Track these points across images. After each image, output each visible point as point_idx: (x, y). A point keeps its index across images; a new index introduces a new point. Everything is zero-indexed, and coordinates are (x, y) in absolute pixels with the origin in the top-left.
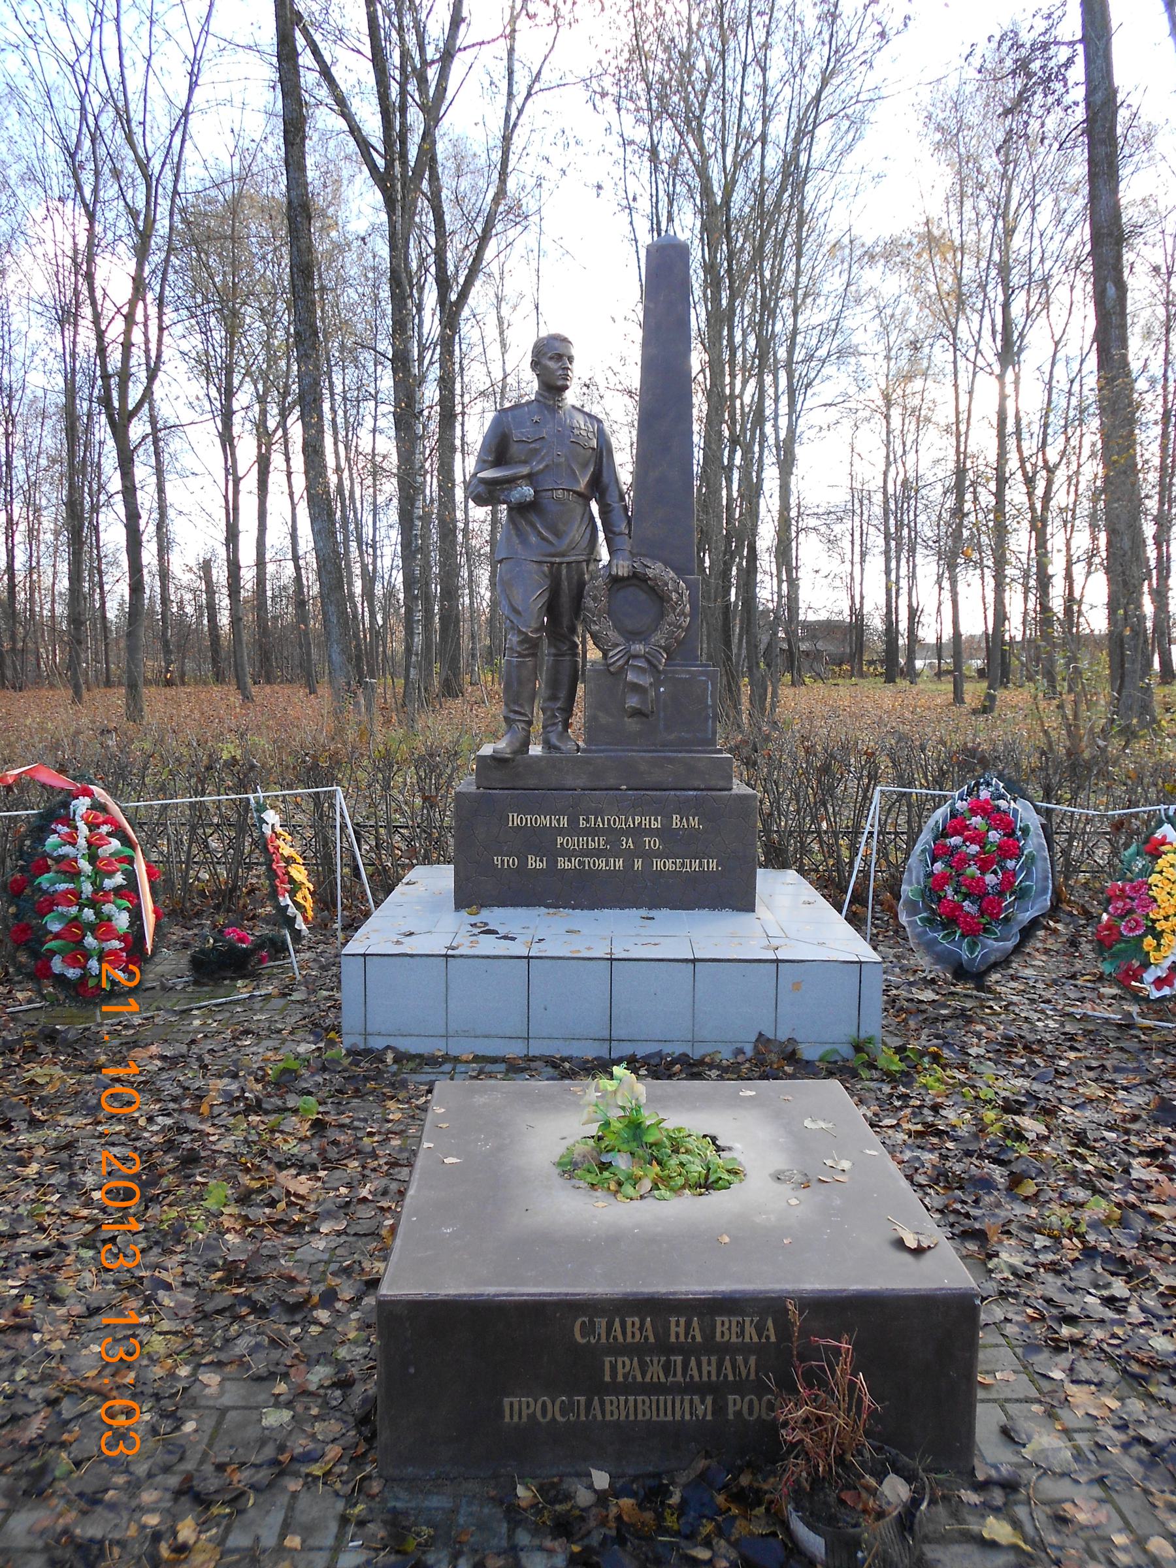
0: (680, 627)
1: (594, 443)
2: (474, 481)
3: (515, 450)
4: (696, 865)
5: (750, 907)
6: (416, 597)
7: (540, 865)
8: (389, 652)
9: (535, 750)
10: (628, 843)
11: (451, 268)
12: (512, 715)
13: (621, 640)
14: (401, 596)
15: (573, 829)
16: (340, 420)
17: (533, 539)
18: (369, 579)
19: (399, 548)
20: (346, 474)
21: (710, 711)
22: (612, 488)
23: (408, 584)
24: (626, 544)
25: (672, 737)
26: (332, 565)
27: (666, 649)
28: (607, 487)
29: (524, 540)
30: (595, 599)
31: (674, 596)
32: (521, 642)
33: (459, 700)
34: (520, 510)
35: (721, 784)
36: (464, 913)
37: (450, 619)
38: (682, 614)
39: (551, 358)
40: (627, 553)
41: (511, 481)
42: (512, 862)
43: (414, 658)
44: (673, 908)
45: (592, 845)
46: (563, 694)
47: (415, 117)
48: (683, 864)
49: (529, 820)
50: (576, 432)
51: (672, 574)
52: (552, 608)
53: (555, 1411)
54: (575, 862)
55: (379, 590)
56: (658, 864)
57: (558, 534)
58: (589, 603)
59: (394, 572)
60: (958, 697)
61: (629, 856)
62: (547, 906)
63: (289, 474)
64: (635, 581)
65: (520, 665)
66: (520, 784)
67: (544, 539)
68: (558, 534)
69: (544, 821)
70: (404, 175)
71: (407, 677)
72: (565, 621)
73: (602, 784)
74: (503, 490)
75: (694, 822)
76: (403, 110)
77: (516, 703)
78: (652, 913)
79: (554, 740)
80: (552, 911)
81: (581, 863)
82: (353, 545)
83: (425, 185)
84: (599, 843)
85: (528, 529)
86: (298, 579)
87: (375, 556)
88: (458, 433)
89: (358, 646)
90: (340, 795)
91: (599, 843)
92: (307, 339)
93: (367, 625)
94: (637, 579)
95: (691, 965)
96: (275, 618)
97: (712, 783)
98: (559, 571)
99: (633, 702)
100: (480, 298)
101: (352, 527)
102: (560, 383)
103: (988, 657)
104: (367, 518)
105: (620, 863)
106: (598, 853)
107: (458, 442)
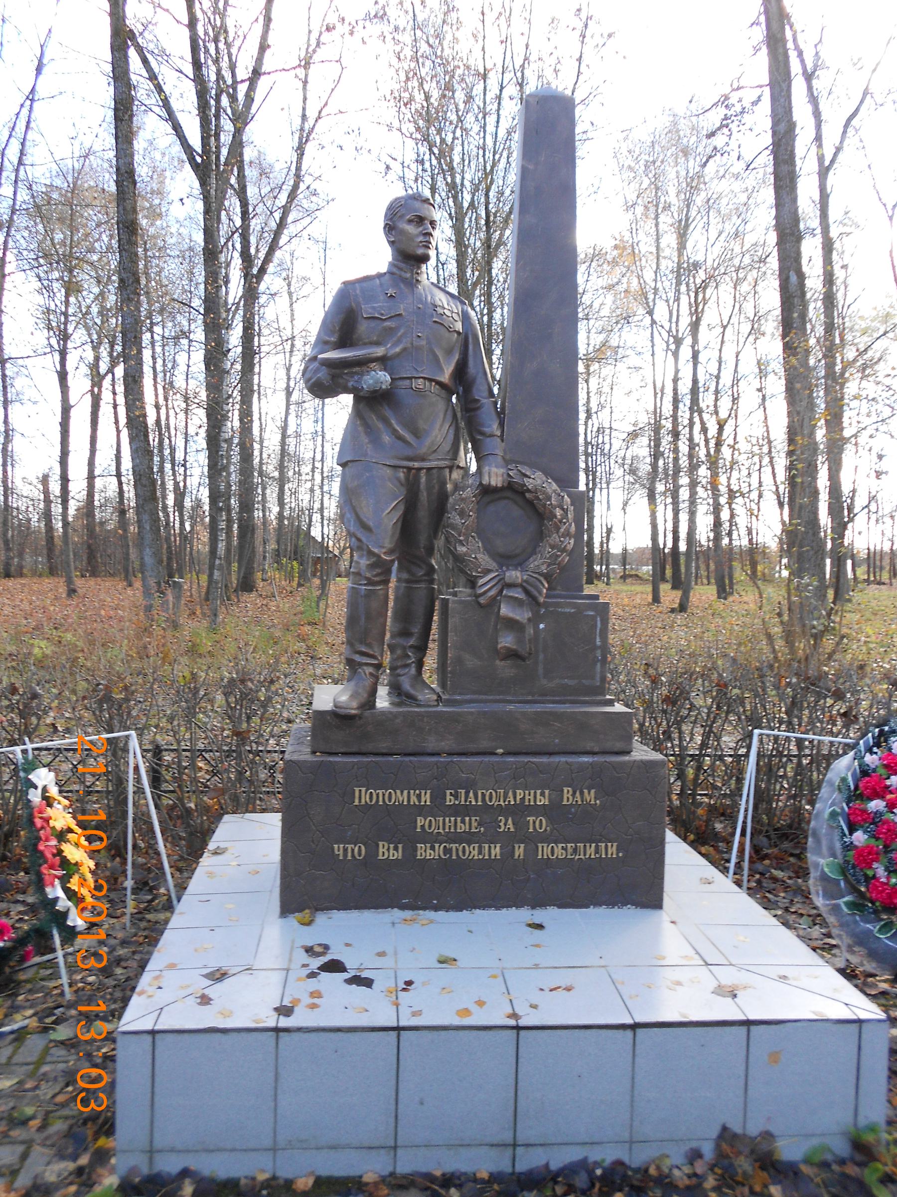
0: (564, 550)
1: (459, 326)
2: (315, 365)
3: (363, 328)
4: (591, 850)
5: (656, 903)
6: (221, 509)
7: (396, 855)
8: (195, 554)
9: (383, 701)
10: (507, 825)
11: (253, 251)
12: (357, 658)
13: (493, 565)
14: (206, 507)
15: (438, 807)
16: (159, 368)
17: (387, 438)
18: (180, 495)
19: (206, 469)
20: (163, 411)
21: (599, 653)
22: (480, 380)
23: (214, 497)
24: (496, 447)
25: (551, 685)
26: (147, 482)
27: (547, 577)
28: (473, 381)
29: (375, 440)
30: (462, 514)
31: (558, 512)
32: (372, 566)
33: (253, 595)
34: (370, 403)
35: (619, 746)
36: (292, 921)
37: (247, 529)
38: (567, 534)
39: (410, 221)
40: (499, 459)
41: (362, 363)
42: (358, 851)
43: (217, 562)
44: (561, 906)
45: (461, 827)
46: (416, 629)
47: (227, 126)
48: (575, 850)
49: (381, 796)
50: (440, 310)
51: (555, 486)
52: (407, 527)
53: (236, 526)
54: (439, 849)
55: (188, 503)
56: (544, 851)
57: (417, 433)
58: (455, 519)
59: (201, 488)
60: (656, 599)
61: (509, 840)
62: (403, 907)
63: (115, 406)
64: (509, 494)
65: (369, 595)
66: (370, 747)
67: (400, 438)
68: (417, 433)
69: (401, 797)
70: (216, 169)
71: (211, 575)
72: (423, 540)
73: (472, 747)
74: (352, 374)
75: (590, 796)
76: (217, 116)
77: (362, 642)
78: (539, 915)
79: (407, 686)
80: (408, 914)
81: (447, 851)
82: (168, 466)
83: (233, 180)
84: (468, 824)
85: (380, 425)
86: (121, 492)
87: (185, 476)
88: (256, 381)
89: (169, 547)
90: (134, 744)
91: (468, 824)
92: (130, 281)
93: (177, 531)
94: (514, 490)
95: (629, 1033)
96: (102, 523)
97: (608, 745)
98: (417, 478)
99: (507, 641)
100: (270, 282)
101: (167, 452)
102: (420, 251)
103: (654, 565)
104: (180, 443)
105: (496, 851)
106: (468, 838)
107: (256, 388)
